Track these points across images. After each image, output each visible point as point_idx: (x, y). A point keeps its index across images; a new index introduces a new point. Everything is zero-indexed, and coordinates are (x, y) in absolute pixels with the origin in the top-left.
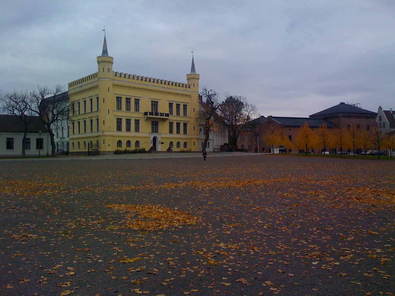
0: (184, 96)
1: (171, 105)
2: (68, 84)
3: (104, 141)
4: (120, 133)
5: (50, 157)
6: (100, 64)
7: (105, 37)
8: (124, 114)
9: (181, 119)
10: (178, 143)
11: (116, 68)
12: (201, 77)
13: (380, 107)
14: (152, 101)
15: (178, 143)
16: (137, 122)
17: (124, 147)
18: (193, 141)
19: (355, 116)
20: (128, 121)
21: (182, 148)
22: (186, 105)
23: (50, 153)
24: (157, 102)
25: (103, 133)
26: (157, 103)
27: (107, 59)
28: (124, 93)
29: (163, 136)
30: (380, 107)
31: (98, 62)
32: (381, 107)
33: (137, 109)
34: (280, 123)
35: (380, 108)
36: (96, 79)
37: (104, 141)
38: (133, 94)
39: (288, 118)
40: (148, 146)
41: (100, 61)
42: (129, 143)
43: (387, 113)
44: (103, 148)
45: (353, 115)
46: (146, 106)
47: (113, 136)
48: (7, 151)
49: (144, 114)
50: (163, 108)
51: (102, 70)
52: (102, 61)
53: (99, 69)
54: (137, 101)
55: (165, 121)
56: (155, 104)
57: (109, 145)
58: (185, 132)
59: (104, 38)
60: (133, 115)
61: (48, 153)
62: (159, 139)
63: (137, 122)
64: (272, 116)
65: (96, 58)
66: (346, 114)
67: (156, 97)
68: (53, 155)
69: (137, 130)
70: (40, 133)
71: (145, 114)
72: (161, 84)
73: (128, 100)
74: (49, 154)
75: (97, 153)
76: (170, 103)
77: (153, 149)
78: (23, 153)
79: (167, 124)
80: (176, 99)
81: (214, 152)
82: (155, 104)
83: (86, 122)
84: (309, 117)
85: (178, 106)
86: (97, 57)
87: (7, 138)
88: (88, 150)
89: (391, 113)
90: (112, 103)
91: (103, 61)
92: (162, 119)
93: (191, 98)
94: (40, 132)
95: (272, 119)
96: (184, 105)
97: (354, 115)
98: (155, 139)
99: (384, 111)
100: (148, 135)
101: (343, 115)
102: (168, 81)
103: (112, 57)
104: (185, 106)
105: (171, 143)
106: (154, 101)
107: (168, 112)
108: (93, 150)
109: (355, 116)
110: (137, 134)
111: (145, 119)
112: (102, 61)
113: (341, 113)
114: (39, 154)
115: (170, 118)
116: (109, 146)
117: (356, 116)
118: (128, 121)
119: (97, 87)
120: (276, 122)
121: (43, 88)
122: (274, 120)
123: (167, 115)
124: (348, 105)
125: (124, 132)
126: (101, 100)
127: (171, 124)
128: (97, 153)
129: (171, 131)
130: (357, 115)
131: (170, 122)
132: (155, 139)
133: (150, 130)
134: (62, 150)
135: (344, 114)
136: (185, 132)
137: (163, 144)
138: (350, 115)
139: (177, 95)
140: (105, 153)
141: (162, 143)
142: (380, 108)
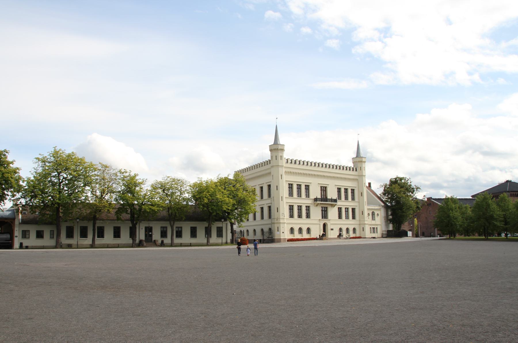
1: (339, 190)
2: (235, 172)
3: (278, 228)
6: (273, 152)
8: (296, 201)
9: (350, 204)
10: (347, 229)
11: (287, 155)
12: (286, 148)
14: (321, 187)
15: (300, 230)
16: (308, 208)
17: (297, 236)
20: (300, 208)
21: (352, 235)
22: (308, 186)
23: (229, 241)
24: (326, 187)
26: (354, 191)
28: (296, 180)
29: (332, 222)
31: (271, 150)
33: (308, 195)
36: (269, 166)
37: (278, 228)
38: (303, 180)
40: (316, 232)
41: (273, 149)
42: (300, 230)
46: (315, 193)
49: (314, 200)
50: (332, 194)
51: (274, 158)
52: (275, 149)
53: (272, 157)
54: (307, 187)
55: (334, 206)
56: (324, 189)
58: (354, 217)
60: (304, 202)
61: (227, 241)
62: (329, 227)
63: (308, 208)
64: (431, 197)
65: (269, 147)
66: (514, 193)
67: (324, 182)
69: (308, 216)
73: (299, 187)
76: (289, 184)
77: (323, 237)
78: (208, 241)
80: (344, 184)
81: (382, 237)
82: (324, 189)
83: (264, 208)
84: (471, 198)
85: (346, 190)
86: (269, 146)
87: (191, 227)
88: (263, 238)
90: (284, 191)
94: (223, 220)
98: (325, 225)
101: (511, 194)
102: (325, 163)
104: (353, 191)
105: (341, 230)
106: (322, 187)
107: (335, 197)
108: (268, 237)
110: (308, 221)
111: (316, 204)
112: (275, 149)
115: (339, 203)
118: (300, 208)
119: (270, 173)
121: (34, 165)
123: (335, 201)
124: (514, 183)
125: (344, 220)
126: (273, 188)
127: (340, 209)
128: (272, 240)
129: (340, 217)
131: (339, 208)
132: (325, 225)
133: (320, 218)
135: (512, 193)
136: (354, 217)
137: (332, 231)
140: (279, 241)
141: (332, 229)
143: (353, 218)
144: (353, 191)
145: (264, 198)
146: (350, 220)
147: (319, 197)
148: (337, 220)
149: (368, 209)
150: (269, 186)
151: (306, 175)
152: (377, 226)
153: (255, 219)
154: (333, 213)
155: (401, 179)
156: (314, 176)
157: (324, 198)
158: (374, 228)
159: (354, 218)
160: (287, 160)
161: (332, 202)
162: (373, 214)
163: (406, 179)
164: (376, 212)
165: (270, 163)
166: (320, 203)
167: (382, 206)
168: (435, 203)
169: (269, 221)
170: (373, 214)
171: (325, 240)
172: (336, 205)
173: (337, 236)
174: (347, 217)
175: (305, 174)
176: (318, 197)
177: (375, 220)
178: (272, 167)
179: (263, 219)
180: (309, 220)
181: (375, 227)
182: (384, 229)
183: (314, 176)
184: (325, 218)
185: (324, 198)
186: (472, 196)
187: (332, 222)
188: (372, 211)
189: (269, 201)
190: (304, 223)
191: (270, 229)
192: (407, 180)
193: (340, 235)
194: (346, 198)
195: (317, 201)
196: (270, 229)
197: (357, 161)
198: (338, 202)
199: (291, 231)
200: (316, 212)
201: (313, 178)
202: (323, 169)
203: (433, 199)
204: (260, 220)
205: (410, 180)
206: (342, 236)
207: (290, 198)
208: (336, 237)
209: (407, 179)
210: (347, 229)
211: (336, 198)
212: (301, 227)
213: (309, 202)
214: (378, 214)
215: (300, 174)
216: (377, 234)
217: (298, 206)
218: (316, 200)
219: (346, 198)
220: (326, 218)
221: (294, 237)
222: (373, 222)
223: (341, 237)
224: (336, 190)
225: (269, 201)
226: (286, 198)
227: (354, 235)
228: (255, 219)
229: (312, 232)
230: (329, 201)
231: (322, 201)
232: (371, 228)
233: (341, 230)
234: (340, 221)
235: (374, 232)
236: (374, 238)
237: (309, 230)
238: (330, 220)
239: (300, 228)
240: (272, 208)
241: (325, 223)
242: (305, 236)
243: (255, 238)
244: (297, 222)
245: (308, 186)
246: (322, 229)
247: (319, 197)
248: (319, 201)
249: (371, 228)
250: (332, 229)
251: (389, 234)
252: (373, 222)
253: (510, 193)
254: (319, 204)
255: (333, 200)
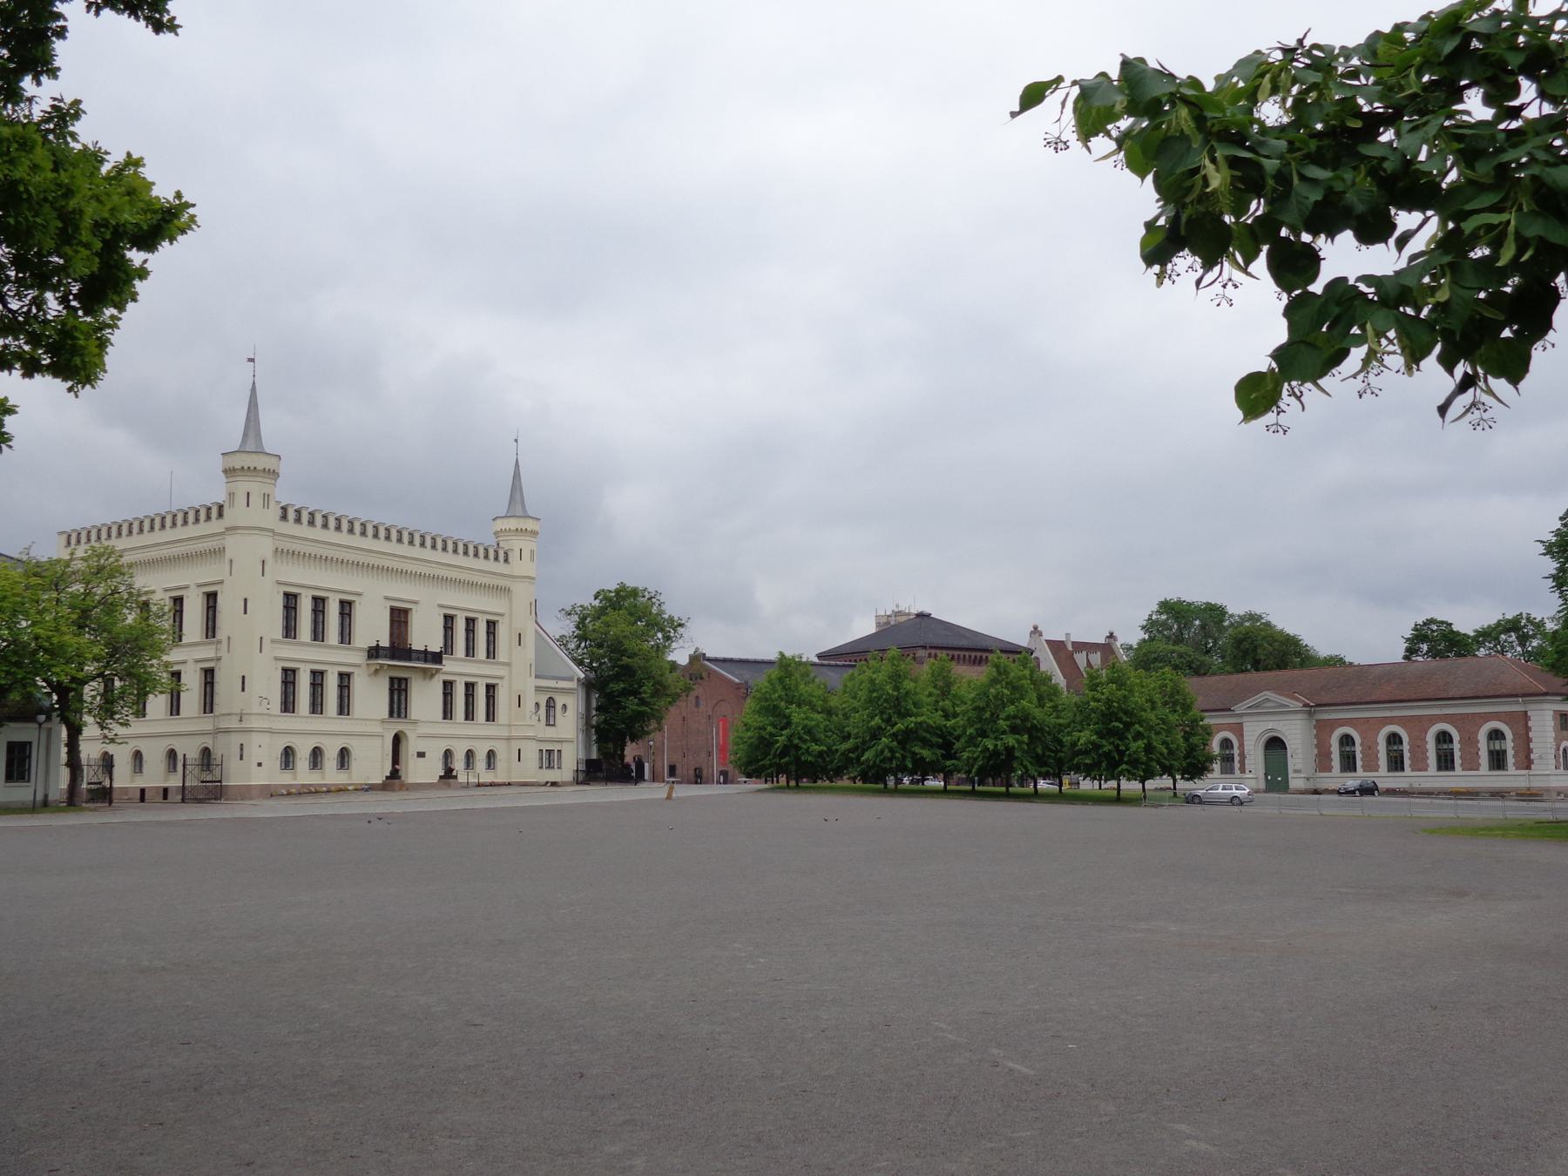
0: (457, 583)
1: (449, 620)
3: (242, 749)
4: (288, 722)
5: (58, 810)
7: (254, 383)
8: (305, 654)
10: (470, 755)
13: (1036, 628)
14: (393, 610)
15: (317, 754)
17: (303, 775)
18: (515, 745)
19: (967, 657)
22: (350, 603)
25: (241, 721)
27: (261, 462)
28: (309, 579)
29: (422, 730)
30: (1036, 628)
31: (229, 472)
32: (1039, 629)
33: (346, 636)
34: (737, 680)
35: (1036, 631)
36: (216, 526)
37: (242, 749)
38: (334, 583)
39: (756, 662)
40: (371, 764)
43: (1056, 647)
44: (236, 775)
45: (962, 653)
46: (373, 628)
47: (271, 732)
48: (1243, 770)
50: (425, 634)
52: (246, 468)
54: (346, 608)
55: (432, 676)
56: (399, 618)
57: (260, 765)
59: (250, 387)
60: (332, 657)
62: (412, 746)
63: (345, 680)
67: (403, 592)
68: (72, 799)
69: (344, 708)
70: (40, 725)
71: (369, 651)
72: (337, 533)
74: (50, 798)
75: (215, 792)
79: (436, 688)
80: (465, 602)
82: (399, 618)
84: (816, 660)
85: (319, 604)
89: (1070, 648)
91: (269, 470)
92: (424, 670)
93: (510, 599)
95: (708, 663)
96: (315, 599)
97: (964, 656)
98: (397, 740)
99: (1048, 642)
100: (378, 729)
103: (279, 456)
105: (448, 755)
107: (436, 645)
108: (203, 782)
109: (967, 657)
110: (343, 724)
111: (373, 669)
112: (246, 468)
113: (924, 647)
114: (32, 798)
115: (449, 666)
116: (259, 768)
117: (970, 656)
119: (219, 552)
120: (722, 675)
122: (713, 666)
123: (437, 658)
127: (448, 686)
128: (215, 792)
129: (448, 713)
130: (973, 654)
131: (445, 683)
134: (100, 783)
138: (981, 657)
139: (290, 556)
140: (245, 793)
141: (421, 755)
142: (1036, 631)
143: (341, 712)
144: (491, 626)
145: (185, 640)
146: (459, 723)
147: (385, 643)
148: (280, 716)
149: (538, 689)
150: (211, 598)
151: (329, 562)
152: (560, 744)
153: (175, 708)
154: (425, 698)
155: (634, 593)
156: (437, 582)
157: (398, 648)
158: (549, 752)
159: (491, 717)
160: (284, 509)
161: (426, 661)
162: (550, 704)
163: (646, 593)
164: (560, 701)
165: (220, 515)
166: (389, 665)
167: (579, 680)
168: (715, 671)
169: (207, 724)
170: (550, 704)
171: (400, 789)
172: (438, 671)
173: (438, 778)
174: (317, 706)
175: (472, 585)
176: (381, 645)
177: (554, 725)
178: (231, 529)
179: (178, 714)
180: (346, 721)
181: (556, 747)
182: (582, 756)
183: (463, 587)
184: (399, 716)
185: (398, 648)
186: (820, 656)
187: (422, 730)
188: (547, 697)
189: (207, 652)
190: (328, 730)
191: (206, 752)
192: (647, 596)
193: (449, 774)
194: (318, 634)
195: (377, 657)
196: (206, 752)
197: (234, 470)
198: (444, 662)
199: (283, 760)
200: (371, 696)
201: (493, 598)
202: (331, 536)
203: (709, 660)
204: (162, 716)
205: (658, 597)
206: (456, 777)
207: (344, 648)
208: (436, 780)
209: (649, 593)
210: (470, 755)
211: (438, 651)
212: (452, 748)
213: (352, 658)
214: (565, 706)
215: (403, 573)
216: (559, 770)
217: (314, 673)
218: (374, 652)
219: (470, 650)
220: (403, 715)
221: (295, 779)
222: (550, 733)
223: (451, 781)
224: (279, 602)
225: (207, 652)
226: (273, 641)
227: (487, 777)
228: (175, 708)
229: (354, 764)
230: (418, 659)
231: (393, 658)
232: (541, 751)
233: (448, 755)
234: (447, 728)
235: (550, 767)
236: (554, 784)
237: (344, 756)
238: (415, 722)
239: (343, 748)
240: (220, 678)
241: (401, 735)
242: (331, 774)
243: (140, 782)
244: (304, 729)
245: (406, 612)
246: (387, 755)
247: (385, 643)
248: (386, 657)
249: (541, 751)
250: (421, 755)
251: (597, 771)
252: (550, 733)
253: (928, 651)
254: (385, 667)
255: (429, 656)
